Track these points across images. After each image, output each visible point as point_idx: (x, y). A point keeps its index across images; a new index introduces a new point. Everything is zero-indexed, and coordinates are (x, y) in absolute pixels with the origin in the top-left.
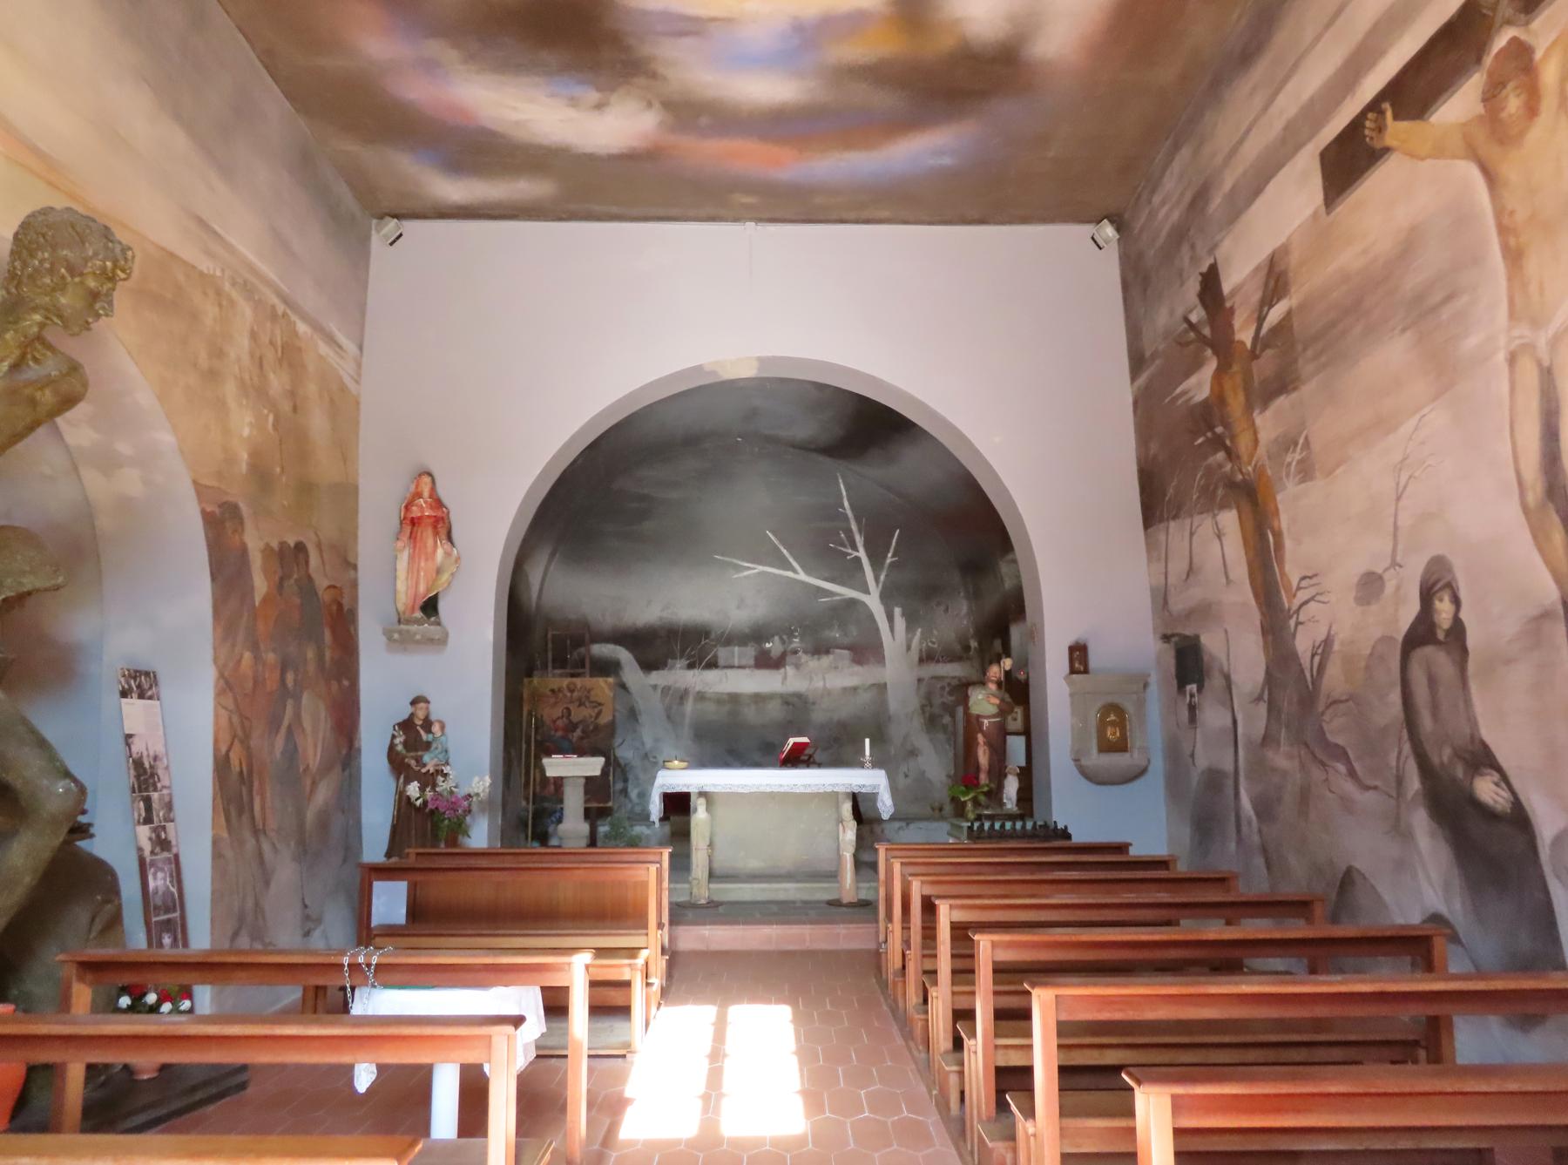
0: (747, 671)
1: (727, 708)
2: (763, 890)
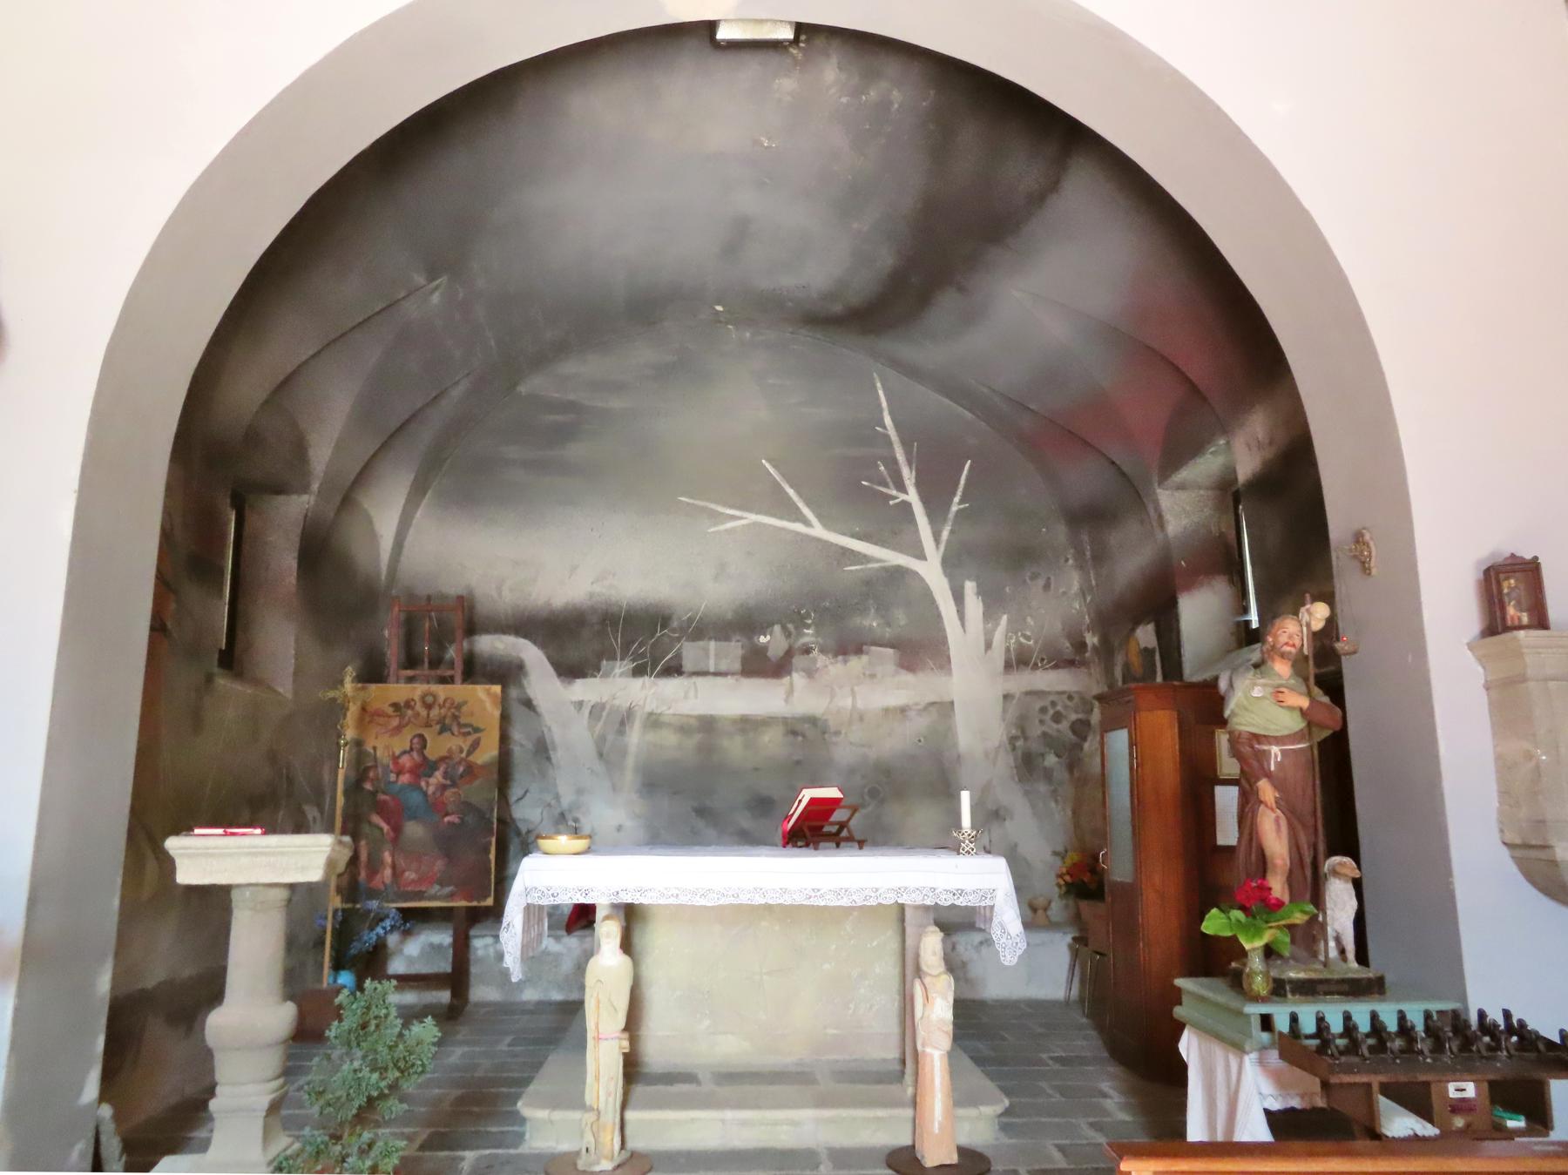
0: (730, 680)
1: (697, 738)
2: (744, 1123)
